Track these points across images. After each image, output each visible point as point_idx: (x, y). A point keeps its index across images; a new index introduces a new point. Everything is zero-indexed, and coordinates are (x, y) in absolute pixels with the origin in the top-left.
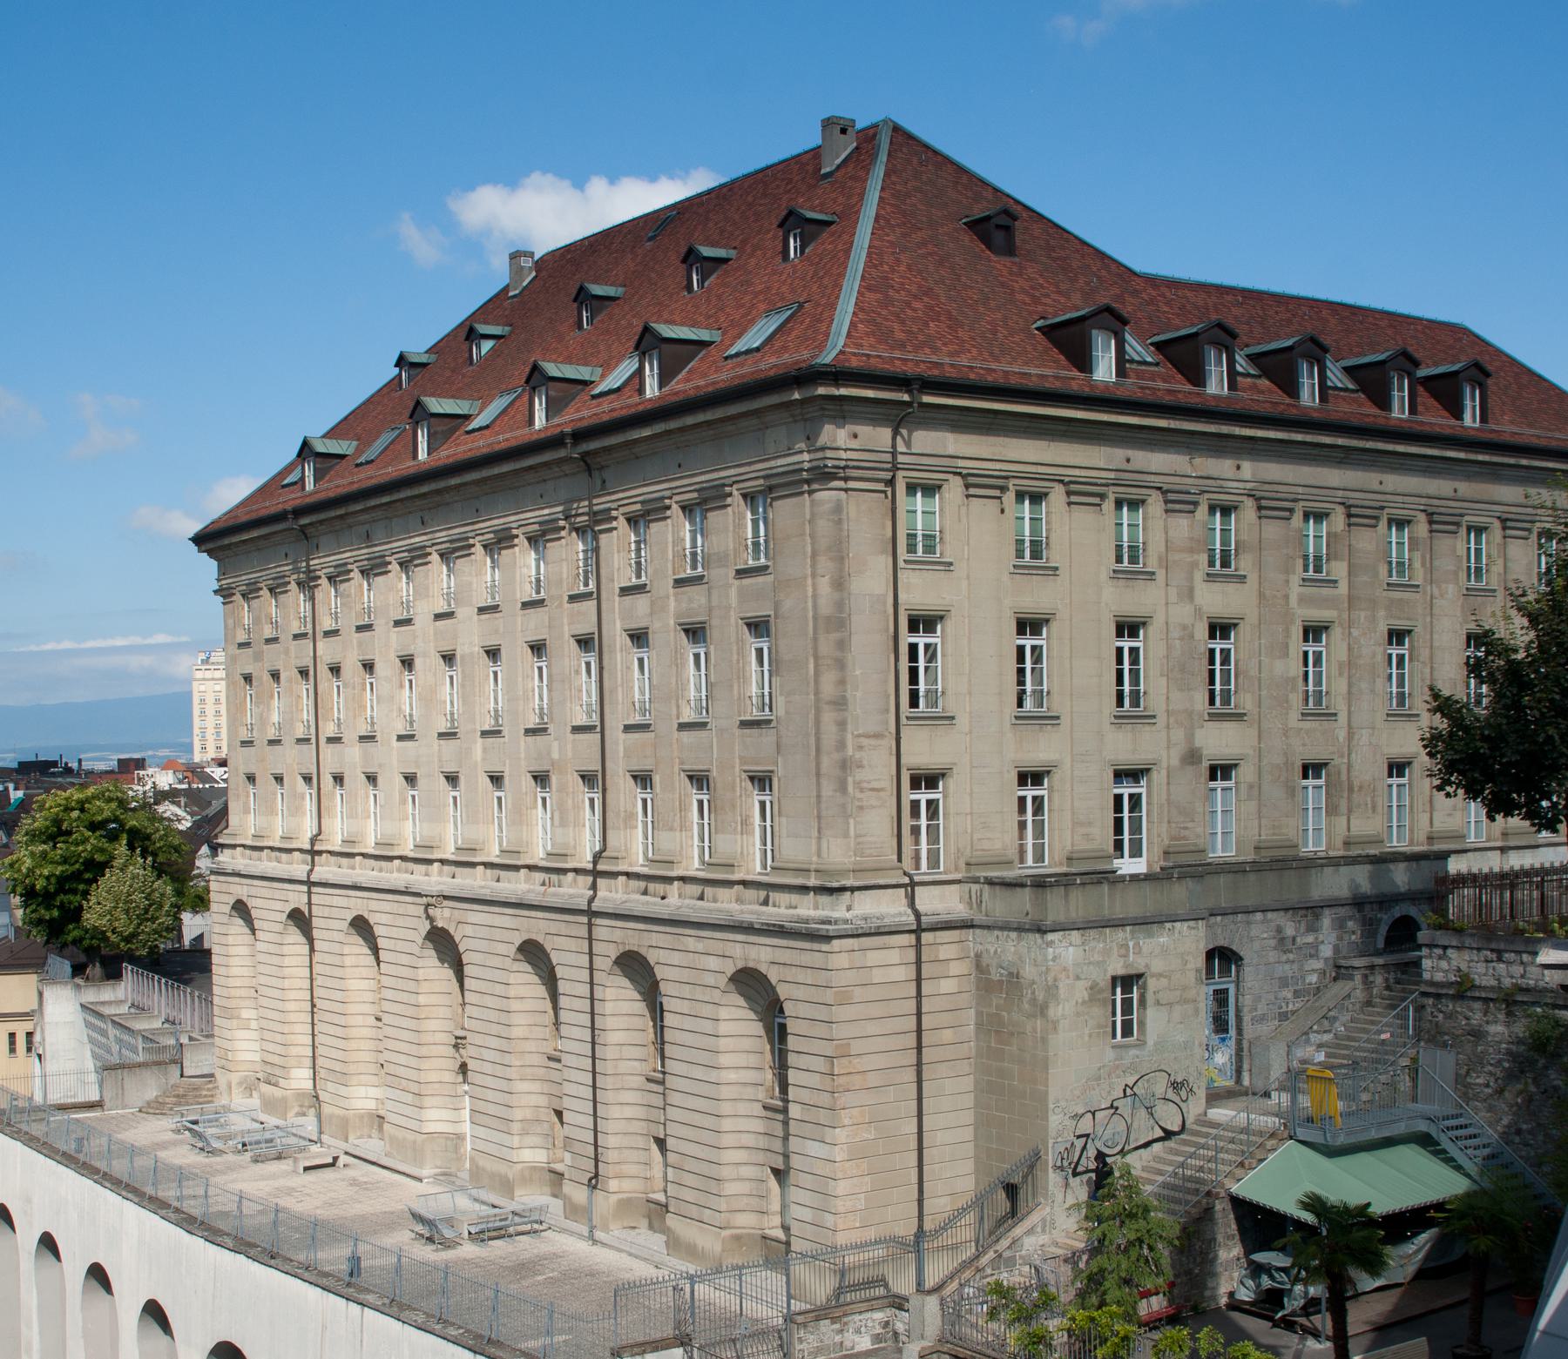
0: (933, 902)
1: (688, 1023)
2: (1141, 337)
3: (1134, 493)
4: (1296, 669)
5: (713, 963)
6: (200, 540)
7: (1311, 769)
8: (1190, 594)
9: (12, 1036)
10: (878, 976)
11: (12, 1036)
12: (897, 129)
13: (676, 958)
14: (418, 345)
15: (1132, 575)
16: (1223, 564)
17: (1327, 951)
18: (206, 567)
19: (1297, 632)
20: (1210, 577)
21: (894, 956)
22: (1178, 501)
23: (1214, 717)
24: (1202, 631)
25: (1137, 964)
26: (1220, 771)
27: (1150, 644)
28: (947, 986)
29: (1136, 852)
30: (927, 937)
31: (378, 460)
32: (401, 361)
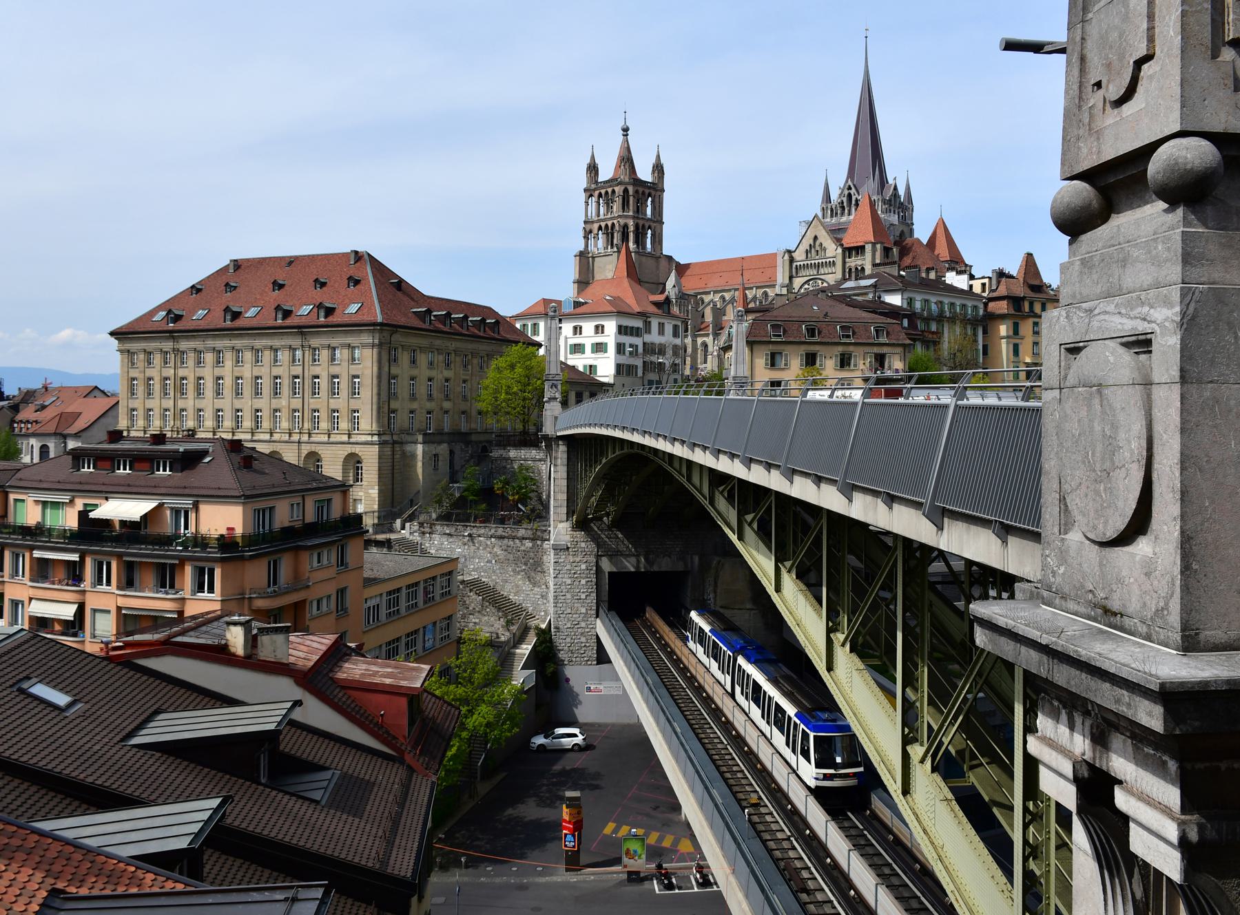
0: (395, 438)
6: (112, 334)
7: (463, 413)
18: (114, 342)
26: (446, 412)
27: (434, 384)
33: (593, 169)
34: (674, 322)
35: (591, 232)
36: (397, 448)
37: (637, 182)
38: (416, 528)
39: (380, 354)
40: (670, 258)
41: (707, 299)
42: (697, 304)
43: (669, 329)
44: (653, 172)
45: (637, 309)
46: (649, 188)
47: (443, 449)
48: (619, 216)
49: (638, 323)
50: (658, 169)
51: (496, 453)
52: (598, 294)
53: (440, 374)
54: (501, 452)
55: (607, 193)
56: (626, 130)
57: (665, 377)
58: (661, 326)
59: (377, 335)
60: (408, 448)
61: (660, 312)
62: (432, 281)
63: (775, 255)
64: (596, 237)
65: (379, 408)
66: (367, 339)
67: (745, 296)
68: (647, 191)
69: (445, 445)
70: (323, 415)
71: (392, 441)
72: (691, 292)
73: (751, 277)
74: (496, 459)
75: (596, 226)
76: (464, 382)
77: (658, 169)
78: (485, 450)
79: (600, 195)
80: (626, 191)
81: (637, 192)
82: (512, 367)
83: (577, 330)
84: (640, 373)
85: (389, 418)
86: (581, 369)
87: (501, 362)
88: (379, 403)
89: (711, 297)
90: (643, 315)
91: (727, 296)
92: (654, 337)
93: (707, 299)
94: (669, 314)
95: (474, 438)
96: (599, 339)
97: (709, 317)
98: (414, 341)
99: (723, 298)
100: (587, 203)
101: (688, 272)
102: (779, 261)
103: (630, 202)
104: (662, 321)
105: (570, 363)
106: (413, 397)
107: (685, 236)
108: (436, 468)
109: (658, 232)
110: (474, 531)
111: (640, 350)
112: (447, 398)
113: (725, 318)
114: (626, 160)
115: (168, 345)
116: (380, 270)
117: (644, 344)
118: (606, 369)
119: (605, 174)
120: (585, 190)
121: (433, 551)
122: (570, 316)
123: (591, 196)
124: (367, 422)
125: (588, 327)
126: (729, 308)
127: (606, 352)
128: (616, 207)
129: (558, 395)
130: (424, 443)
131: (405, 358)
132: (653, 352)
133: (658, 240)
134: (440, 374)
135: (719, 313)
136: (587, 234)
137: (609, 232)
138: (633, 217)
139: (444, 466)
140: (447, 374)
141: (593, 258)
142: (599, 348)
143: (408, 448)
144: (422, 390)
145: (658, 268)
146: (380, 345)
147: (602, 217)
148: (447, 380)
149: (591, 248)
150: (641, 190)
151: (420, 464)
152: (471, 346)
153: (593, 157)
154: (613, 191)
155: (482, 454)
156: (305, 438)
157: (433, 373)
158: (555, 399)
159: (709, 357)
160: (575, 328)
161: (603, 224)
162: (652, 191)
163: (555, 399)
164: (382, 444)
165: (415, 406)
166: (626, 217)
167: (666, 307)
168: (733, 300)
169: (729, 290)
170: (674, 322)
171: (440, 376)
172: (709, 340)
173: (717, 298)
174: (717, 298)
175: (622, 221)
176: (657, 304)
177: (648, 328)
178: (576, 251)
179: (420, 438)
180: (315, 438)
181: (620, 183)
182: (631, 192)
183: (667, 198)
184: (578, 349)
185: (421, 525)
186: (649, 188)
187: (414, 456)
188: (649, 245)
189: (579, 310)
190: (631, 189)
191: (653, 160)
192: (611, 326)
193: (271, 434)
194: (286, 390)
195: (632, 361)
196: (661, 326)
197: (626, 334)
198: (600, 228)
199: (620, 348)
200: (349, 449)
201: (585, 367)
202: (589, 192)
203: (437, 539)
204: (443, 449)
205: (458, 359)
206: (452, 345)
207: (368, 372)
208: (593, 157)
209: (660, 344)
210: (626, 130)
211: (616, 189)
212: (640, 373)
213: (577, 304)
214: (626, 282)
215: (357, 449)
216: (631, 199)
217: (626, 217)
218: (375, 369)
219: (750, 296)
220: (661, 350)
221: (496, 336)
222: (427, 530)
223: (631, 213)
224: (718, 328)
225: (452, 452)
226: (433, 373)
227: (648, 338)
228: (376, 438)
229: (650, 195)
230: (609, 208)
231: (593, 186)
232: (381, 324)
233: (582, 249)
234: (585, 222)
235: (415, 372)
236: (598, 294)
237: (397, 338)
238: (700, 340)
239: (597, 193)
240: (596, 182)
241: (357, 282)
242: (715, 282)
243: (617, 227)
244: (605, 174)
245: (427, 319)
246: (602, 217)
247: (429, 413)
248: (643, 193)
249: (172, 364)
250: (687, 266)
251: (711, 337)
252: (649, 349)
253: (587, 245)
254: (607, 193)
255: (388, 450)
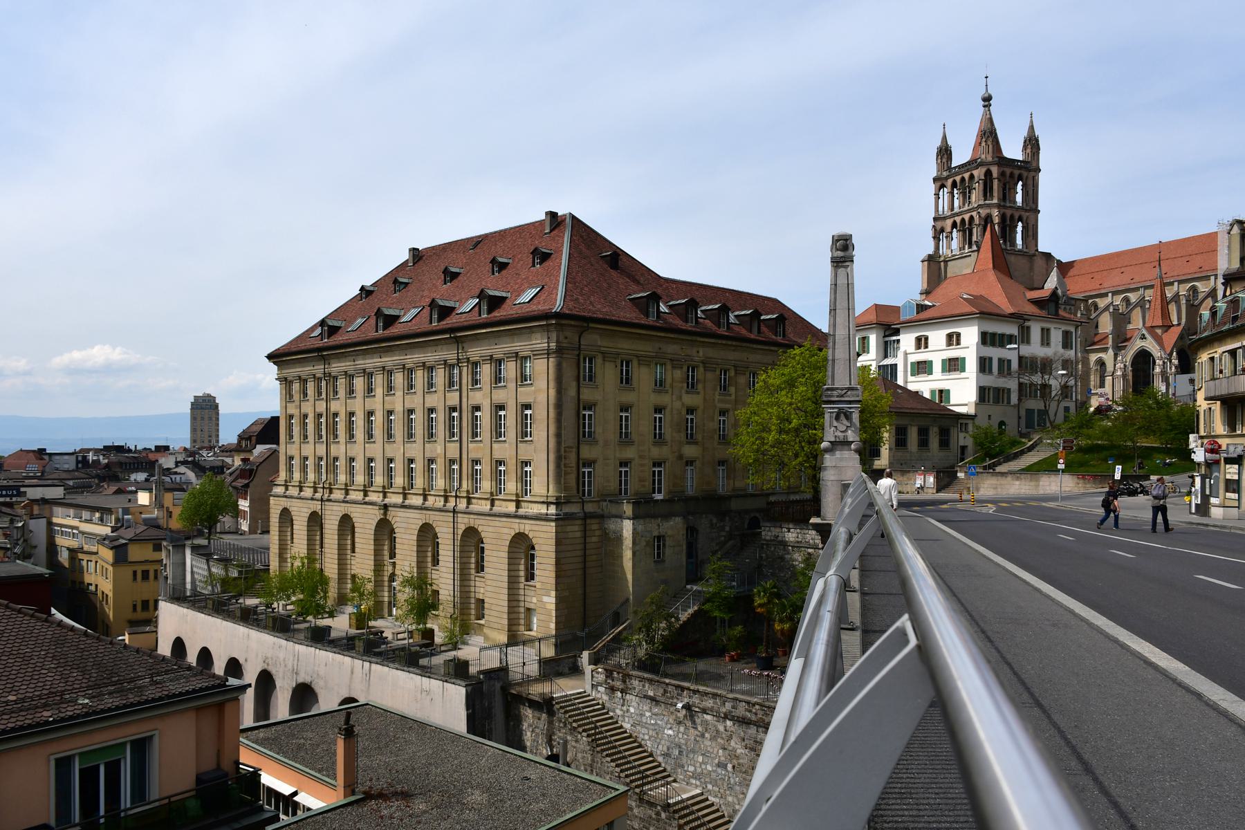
0: (590, 508)
1: (495, 553)
2: (665, 303)
3: (663, 361)
4: (716, 424)
5: (506, 531)
6: (270, 357)
7: (722, 463)
8: (680, 398)
9: (135, 573)
10: (571, 535)
11: (135, 573)
12: (574, 218)
13: (491, 529)
14: (368, 283)
15: (660, 392)
16: (692, 387)
17: (727, 529)
18: (273, 369)
19: (717, 413)
20: (687, 392)
21: (576, 528)
22: (676, 363)
23: (688, 443)
24: (684, 412)
25: (662, 531)
26: (690, 462)
27: (667, 417)
28: (594, 539)
29: (660, 492)
30: (588, 521)
31: (357, 327)
32: (362, 288)
33: (945, 152)
34: (1064, 328)
35: (942, 230)
36: (594, 525)
37: (1003, 162)
38: (601, 677)
39: (559, 368)
40: (1048, 256)
41: (1102, 303)
42: (1087, 309)
43: (1056, 336)
44: (1025, 147)
45: (1009, 309)
46: (1020, 168)
47: (674, 527)
48: (980, 206)
49: (1012, 330)
50: (1032, 143)
51: (768, 533)
52: (952, 293)
53: (678, 400)
54: (775, 531)
55: (963, 179)
56: (987, 99)
57: (1053, 405)
58: (1046, 333)
59: (554, 336)
60: (611, 525)
61: (1043, 313)
62: (669, 254)
63: (1212, 237)
64: (949, 237)
65: (559, 459)
66: (539, 342)
67: (1163, 294)
68: (1017, 172)
69: (678, 520)
70: (485, 468)
71: (580, 514)
72: (1080, 296)
73: (1172, 269)
74: (768, 543)
75: (949, 222)
76: (723, 413)
77: (1032, 143)
78: (755, 524)
79: (954, 185)
80: (988, 173)
81: (1002, 174)
82: (791, 384)
83: (921, 343)
84: (1014, 399)
85: (580, 477)
86: (927, 395)
87: (774, 377)
88: (558, 450)
89: (1109, 299)
90: (1017, 317)
91: (1133, 297)
92: (1035, 349)
93: (1102, 303)
94: (1056, 317)
95: (735, 505)
96: (954, 353)
97: (1106, 325)
98: (625, 346)
99: (1127, 300)
100: (937, 195)
101: (1071, 273)
102: (1222, 242)
103: (994, 191)
104: (1046, 325)
105: (912, 387)
106: (625, 439)
107: (1073, 224)
108: (660, 559)
109: (1031, 223)
110: (696, 700)
111: (1015, 365)
112: (691, 439)
113: (1130, 327)
114: (989, 134)
115: (318, 369)
116: (583, 234)
117: (1020, 358)
118: (963, 394)
119: (960, 157)
120: (935, 180)
121: (627, 726)
122: (911, 324)
123: (943, 186)
124: (542, 484)
125: (937, 337)
126: (1137, 315)
127: (963, 370)
128: (976, 197)
129: (851, 435)
130: (634, 518)
131: (608, 374)
132: (1033, 370)
133: (1031, 233)
134: (678, 400)
135: (1121, 319)
136: (938, 233)
137: (965, 228)
138: (998, 206)
139: (675, 555)
140: (689, 400)
141: (946, 262)
142: (953, 365)
143: (611, 525)
144: (642, 426)
145: (1031, 269)
146: (560, 351)
147: (956, 210)
148: (690, 411)
149: (944, 251)
150: (1008, 171)
151: (628, 555)
152: (733, 356)
153: (945, 138)
154: (972, 177)
155: (747, 533)
156: (462, 505)
157: (664, 399)
158: (845, 443)
159: (1108, 380)
160: (918, 340)
161: (958, 219)
162: (1025, 171)
163: (845, 443)
164: (560, 520)
165: (629, 453)
166: (989, 206)
167: (1052, 306)
168: (1141, 303)
169: (1136, 289)
170: (1064, 328)
171: (677, 405)
172: (1108, 357)
173: (1118, 300)
174: (1118, 300)
175: (983, 212)
176: (1038, 303)
177: (1025, 337)
178: (924, 255)
179: (628, 509)
180: (475, 507)
181: (982, 164)
182: (995, 174)
183: (1044, 179)
184: (922, 368)
185: (609, 673)
186: (1020, 168)
187: (619, 539)
188: (1019, 241)
189: (924, 316)
190: (995, 171)
191: (1024, 133)
192: (970, 334)
193: (405, 496)
194: (440, 430)
195: (1002, 383)
196: (1046, 333)
197: (993, 344)
198: (954, 225)
199: (984, 365)
200: (517, 526)
201: (933, 392)
202: (940, 182)
203: (634, 705)
204: (674, 527)
205: (709, 375)
206: (699, 353)
207: (542, 398)
208: (945, 138)
209: (1043, 359)
210: (987, 99)
211: (976, 173)
212: (1014, 399)
213: (921, 308)
214: (992, 276)
215: (527, 527)
216: (996, 183)
217: (989, 206)
218: (552, 392)
219: (1169, 295)
220: (1045, 366)
221: (779, 339)
222: (618, 684)
223: (995, 201)
224: (1121, 340)
225: (691, 531)
226: (664, 399)
227: (1026, 350)
228: (552, 510)
229: (1020, 178)
230: (966, 196)
231: (945, 174)
232: (557, 315)
233: (931, 251)
234: (935, 219)
235: (628, 397)
236: (952, 293)
237: (592, 340)
238: (1093, 357)
239: (950, 181)
240: (950, 168)
241: (545, 257)
242: (1116, 280)
243: (977, 221)
244: (960, 157)
245: (653, 310)
246: (956, 210)
247: (657, 464)
248: (1012, 175)
249: (324, 396)
250: (1071, 265)
251: (1111, 352)
252: (1027, 364)
253: (937, 248)
254: (963, 179)
255: (575, 530)
